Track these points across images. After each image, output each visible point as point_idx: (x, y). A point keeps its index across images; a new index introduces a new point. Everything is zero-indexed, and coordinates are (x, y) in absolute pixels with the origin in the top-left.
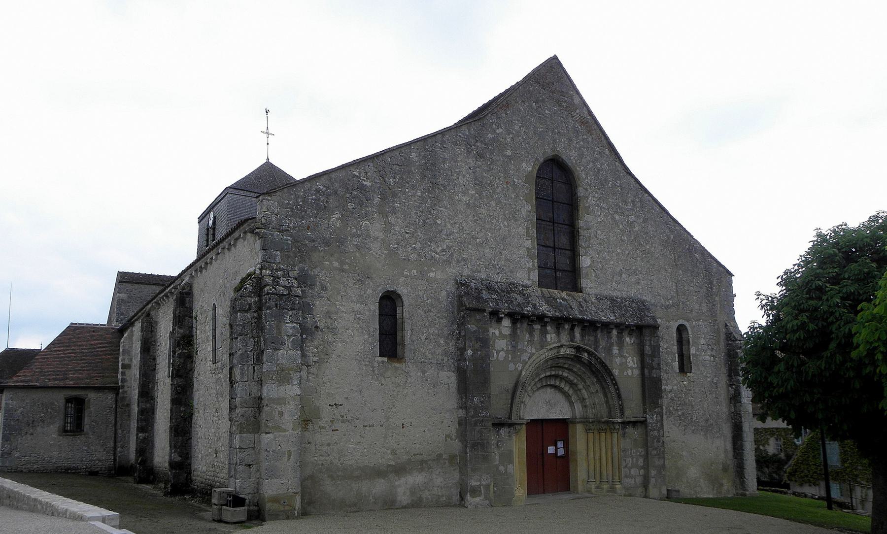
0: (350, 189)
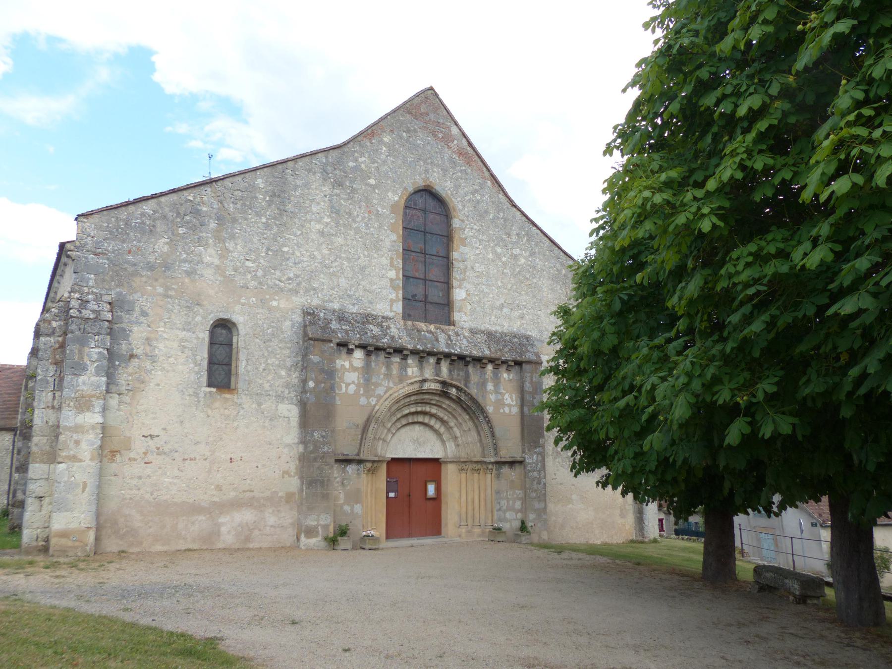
0: (182, 213)
